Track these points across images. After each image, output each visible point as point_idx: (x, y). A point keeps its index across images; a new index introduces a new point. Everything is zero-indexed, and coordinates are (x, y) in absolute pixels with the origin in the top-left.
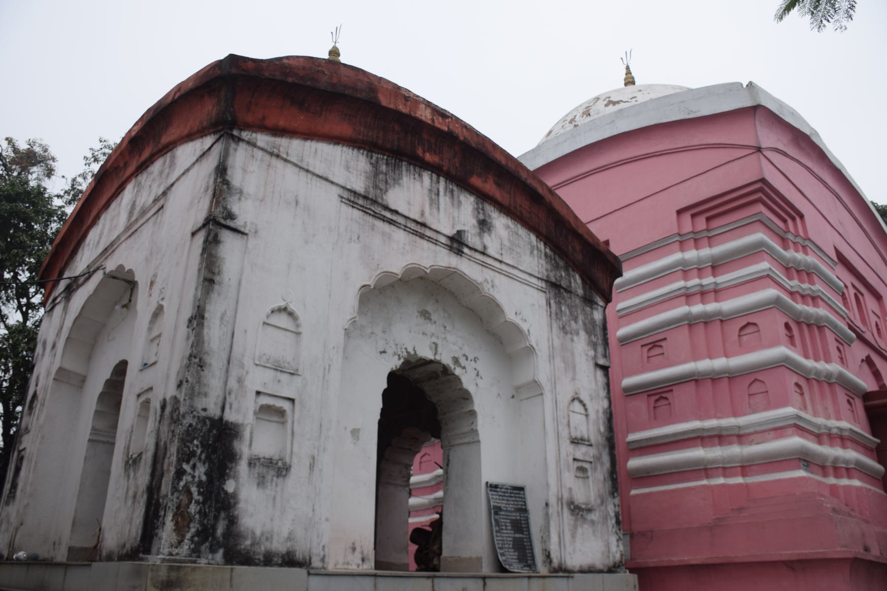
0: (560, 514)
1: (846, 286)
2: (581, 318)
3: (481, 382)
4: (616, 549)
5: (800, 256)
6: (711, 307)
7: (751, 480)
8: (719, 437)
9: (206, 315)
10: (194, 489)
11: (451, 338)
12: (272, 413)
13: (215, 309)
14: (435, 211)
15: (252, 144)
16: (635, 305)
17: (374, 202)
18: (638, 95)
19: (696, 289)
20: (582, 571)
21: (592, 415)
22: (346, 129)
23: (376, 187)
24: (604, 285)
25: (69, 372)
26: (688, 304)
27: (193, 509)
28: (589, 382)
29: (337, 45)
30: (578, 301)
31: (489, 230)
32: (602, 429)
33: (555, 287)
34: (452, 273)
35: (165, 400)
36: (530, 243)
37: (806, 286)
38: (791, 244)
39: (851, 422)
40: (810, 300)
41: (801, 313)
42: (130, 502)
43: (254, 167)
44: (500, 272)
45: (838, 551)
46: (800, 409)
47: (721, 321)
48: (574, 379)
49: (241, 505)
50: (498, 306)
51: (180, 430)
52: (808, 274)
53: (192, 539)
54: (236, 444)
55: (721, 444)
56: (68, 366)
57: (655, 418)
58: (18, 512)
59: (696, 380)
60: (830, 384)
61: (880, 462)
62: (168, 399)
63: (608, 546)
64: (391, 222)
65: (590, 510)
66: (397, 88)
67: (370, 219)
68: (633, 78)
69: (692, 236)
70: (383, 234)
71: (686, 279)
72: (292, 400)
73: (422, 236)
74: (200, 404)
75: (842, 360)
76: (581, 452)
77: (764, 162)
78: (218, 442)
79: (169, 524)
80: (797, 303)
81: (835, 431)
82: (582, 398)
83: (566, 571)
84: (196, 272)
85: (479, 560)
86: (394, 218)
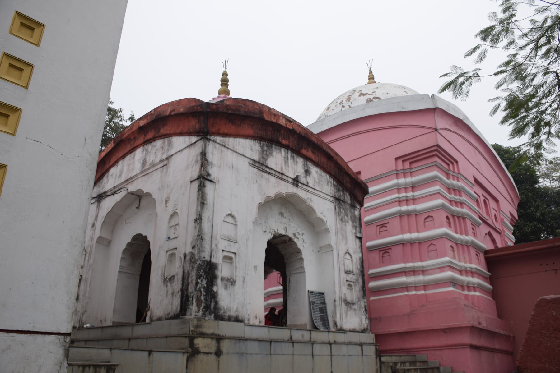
0: (341, 305)
1: (479, 196)
2: (349, 214)
3: (305, 244)
4: (365, 323)
5: (455, 182)
6: (411, 207)
7: (428, 292)
8: (414, 272)
9: (203, 218)
10: (202, 290)
11: (292, 225)
12: (228, 259)
13: (206, 215)
14: (287, 167)
15: (215, 141)
16: (374, 207)
17: (262, 164)
18: (376, 90)
19: (404, 198)
20: (350, 331)
21: (354, 260)
22: (250, 132)
23: (263, 157)
24: (360, 198)
25: (104, 238)
26: (400, 205)
27: (202, 298)
28: (353, 245)
29: (226, 70)
30: (348, 206)
31: (309, 174)
32: (359, 267)
33: (338, 200)
34: (293, 195)
35: (185, 254)
36: (327, 180)
37: (457, 197)
38: (451, 176)
39: (478, 265)
40: (459, 205)
41: (454, 211)
42: (170, 296)
43: (216, 152)
44: (314, 194)
45: (465, 324)
46: (452, 258)
47: (416, 214)
48: (346, 243)
49: (219, 297)
50: (313, 210)
51: (196, 266)
52: (459, 191)
53: (202, 310)
54: (216, 271)
55: (414, 275)
56: (103, 236)
57: (383, 262)
58: (82, 306)
59: (403, 244)
60: (467, 246)
61: (491, 284)
62: (187, 253)
63: (361, 320)
64: (269, 173)
65: (353, 304)
66: (270, 109)
67: (261, 172)
68: (373, 76)
69: (402, 171)
70: (266, 179)
71: (399, 193)
72: (235, 254)
73: (282, 179)
74: (203, 255)
75: (475, 234)
76: (350, 277)
77: (439, 135)
78: (209, 270)
79: (195, 304)
80: (453, 206)
81: (468, 269)
82: (350, 252)
83: (343, 330)
84: (196, 199)
85: (305, 325)
86: (271, 171)
